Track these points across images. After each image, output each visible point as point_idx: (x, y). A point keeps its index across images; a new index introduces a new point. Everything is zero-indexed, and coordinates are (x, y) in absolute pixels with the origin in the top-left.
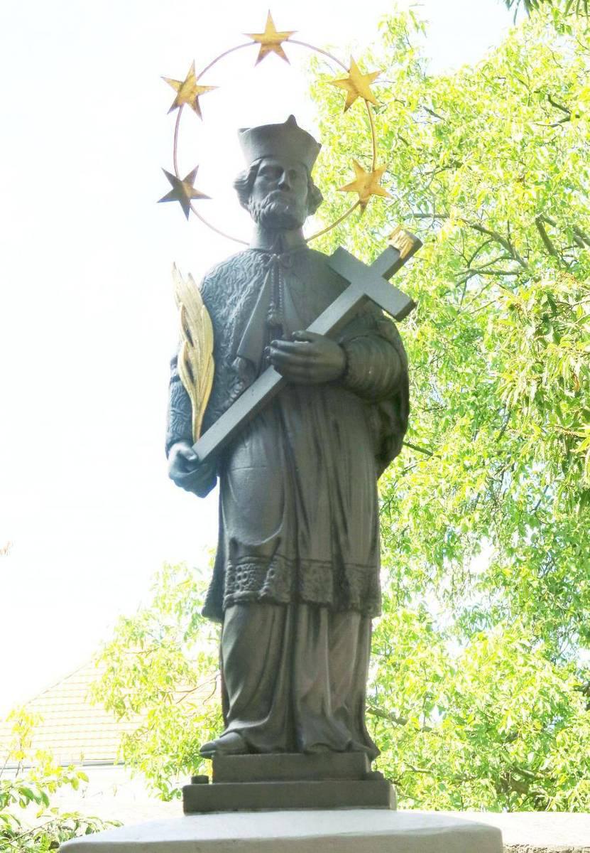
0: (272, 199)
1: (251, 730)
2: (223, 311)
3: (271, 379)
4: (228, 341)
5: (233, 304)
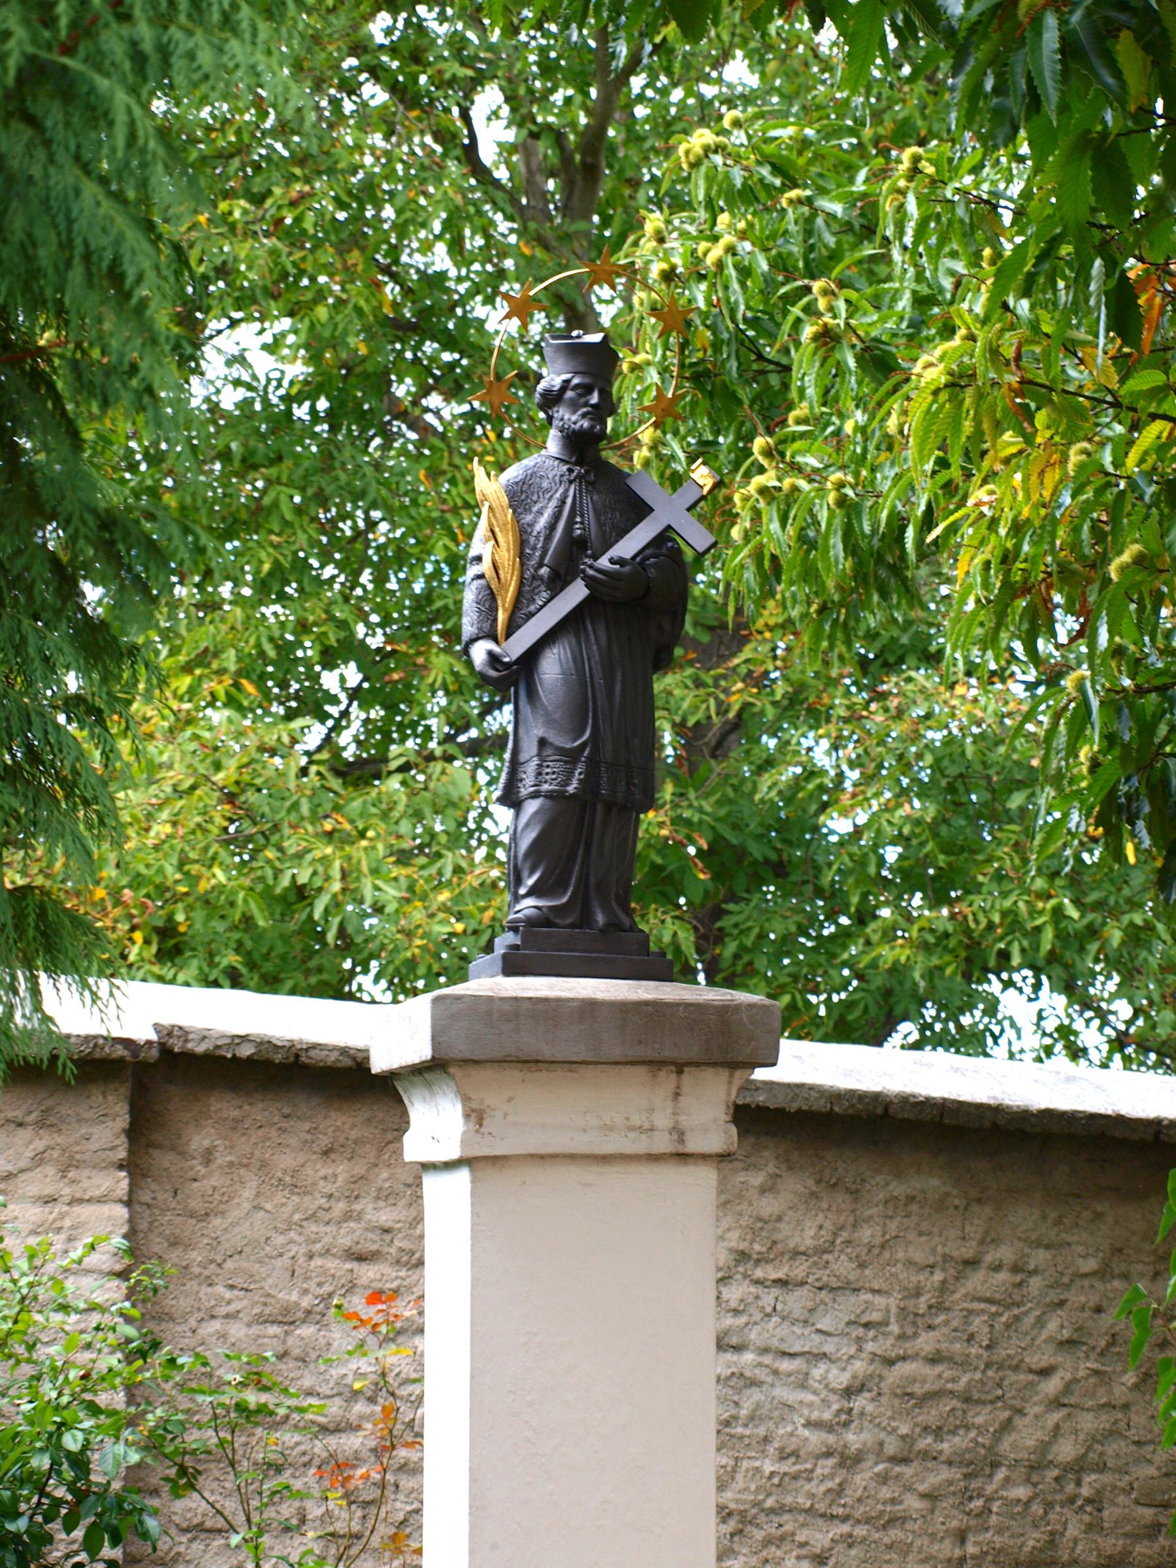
0: (584, 416)
1: (551, 908)
2: (529, 518)
3: (577, 592)
4: (534, 548)
5: (540, 513)
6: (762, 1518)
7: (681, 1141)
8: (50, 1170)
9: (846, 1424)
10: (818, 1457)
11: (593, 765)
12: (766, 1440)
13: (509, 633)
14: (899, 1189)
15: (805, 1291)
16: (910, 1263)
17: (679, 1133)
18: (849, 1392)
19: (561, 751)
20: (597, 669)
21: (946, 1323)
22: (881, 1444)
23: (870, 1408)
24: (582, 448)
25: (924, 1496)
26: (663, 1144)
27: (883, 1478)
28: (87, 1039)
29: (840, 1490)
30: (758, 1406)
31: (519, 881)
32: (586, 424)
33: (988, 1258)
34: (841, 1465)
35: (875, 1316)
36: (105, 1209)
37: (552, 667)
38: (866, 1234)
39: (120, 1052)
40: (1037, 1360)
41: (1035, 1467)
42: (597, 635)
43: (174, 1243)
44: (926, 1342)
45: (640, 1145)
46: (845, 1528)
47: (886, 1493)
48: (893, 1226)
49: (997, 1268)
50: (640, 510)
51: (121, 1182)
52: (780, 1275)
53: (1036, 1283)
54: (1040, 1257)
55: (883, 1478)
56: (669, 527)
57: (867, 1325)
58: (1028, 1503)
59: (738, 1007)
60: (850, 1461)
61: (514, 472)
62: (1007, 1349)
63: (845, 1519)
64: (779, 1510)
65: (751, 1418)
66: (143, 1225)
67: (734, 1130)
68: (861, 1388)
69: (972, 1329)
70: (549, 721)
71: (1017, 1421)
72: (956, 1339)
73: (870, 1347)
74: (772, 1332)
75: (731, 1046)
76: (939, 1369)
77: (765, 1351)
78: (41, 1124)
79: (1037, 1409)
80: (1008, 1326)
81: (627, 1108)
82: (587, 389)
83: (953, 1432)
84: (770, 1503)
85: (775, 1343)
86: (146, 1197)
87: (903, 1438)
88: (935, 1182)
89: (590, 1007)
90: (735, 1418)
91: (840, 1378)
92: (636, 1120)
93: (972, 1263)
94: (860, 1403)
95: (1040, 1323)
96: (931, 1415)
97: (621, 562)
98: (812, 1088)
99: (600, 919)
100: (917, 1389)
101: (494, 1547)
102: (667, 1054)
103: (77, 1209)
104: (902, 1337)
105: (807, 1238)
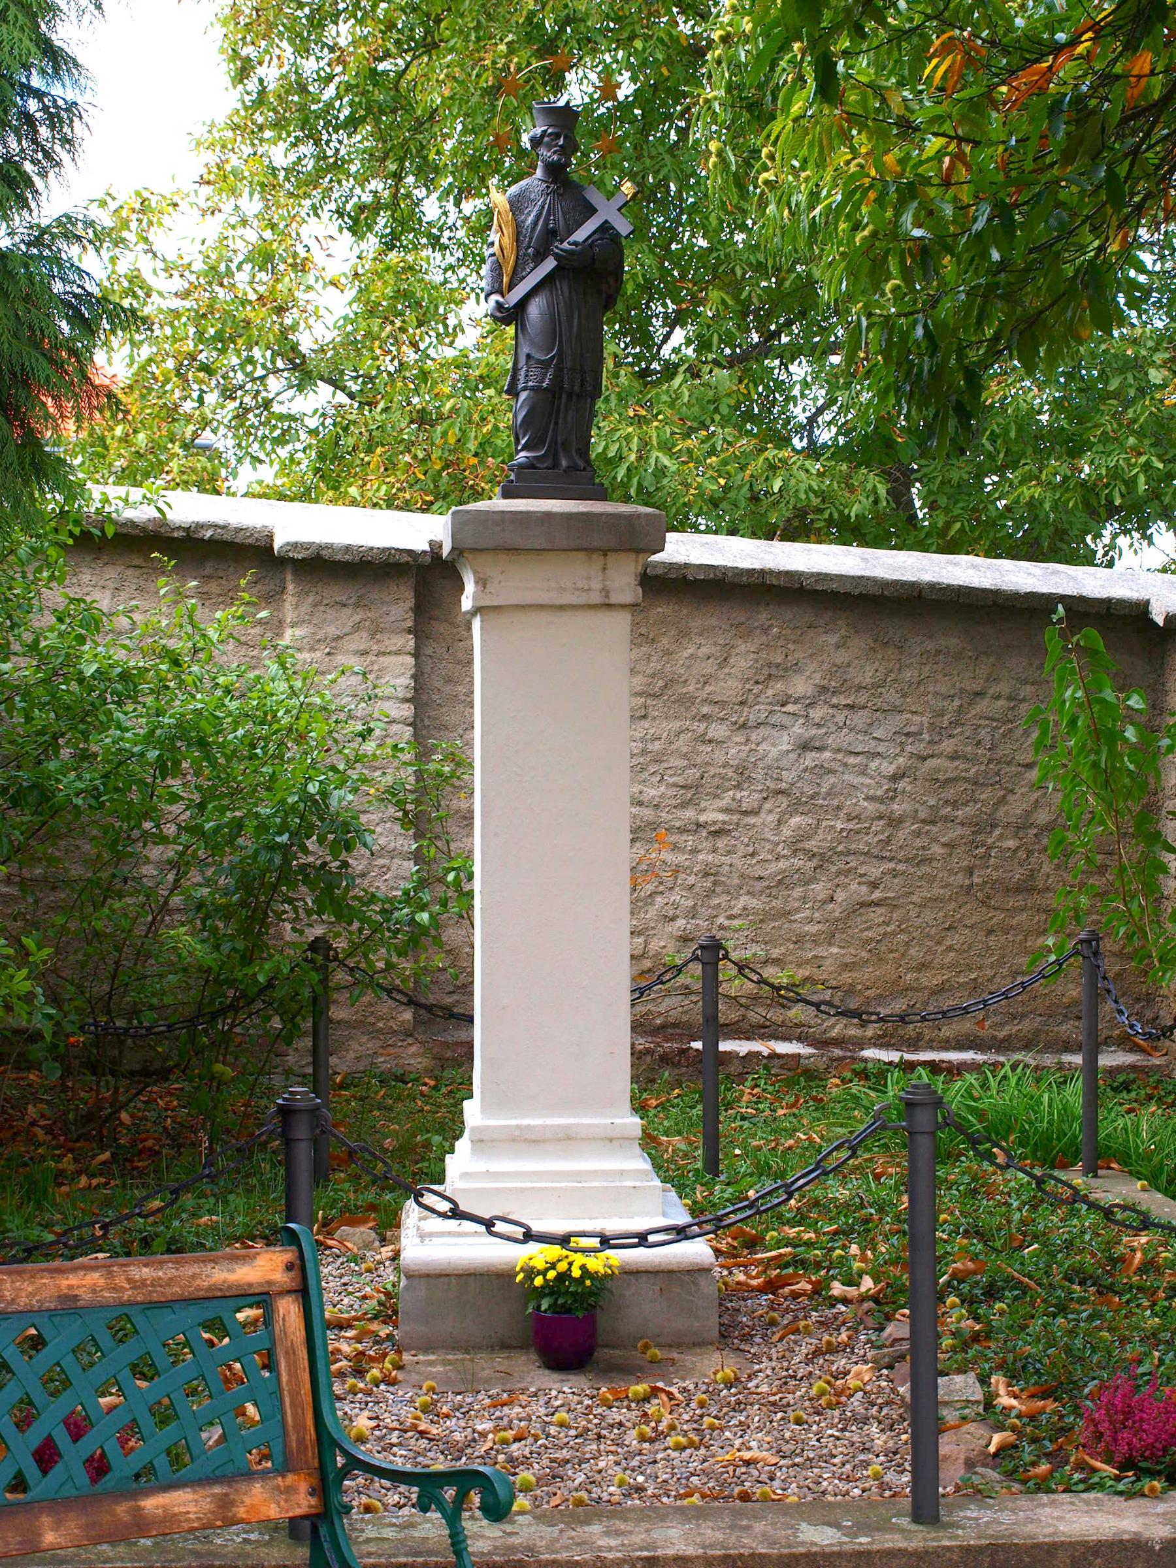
3: (550, 264)
5: (529, 214)
6: (835, 858)
7: (607, 596)
8: (364, 634)
9: (893, 799)
10: (873, 819)
11: (559, 370)
12: (838, 808)
13: (511, 287)
14: (930, 646)
15: (865, 712)
16: (937, 694)
17: (606, 592)
18: (894, 778)
19: (539, 362)
20: (562, 310)
21: (962, 733)
22: (916, 811)
23: (909, 788)
24: (556, 172)
25: (944, 845)
26: (595, 598)
27: (917, 834)
28: (384, 550)
29: (888, 841)
30: (833, 786)
31: (517, 441)
32: (555, 157)
33: (991, 691)
34: (889, 825)
35: (913, 729)
36: (400, 658)
37: (534, 310)
38: (907, 675)
39: (405, 558)
40: (1022, 758)
41: (1021, 826)
42: (563, 287)
43: (448, 681)
44: (947, 746)
45: (582, 599)
46: (891, 865)
47: (919, 843)
48: (926, 671)
49: (998, 697)
50: (591, 211)
51: (410, 642)
52: (849, 702)
53: (1024, 707)
54: (1027, 690)
55: (917, 834)
56: (606, 222)
57: (907, 735)
58: (1016, 851)
59: (639, 516)
60: (895, 822)
61: (514, 189)
62: (1003, 751)
63: (891, 859)
64: (848, 853)
65: (828, 794)
66: (427, 669)
67: (640, 590)
68: (903, 776)
69: (980, 737)
70: (532, 344)
71: (1010, 798)
72: (967, 744)
73: (909, 748)
74: (844, 739)
75: (639, 539)
76: (956, 763)
77: (839, 750)
78: (357, 605)
79: (1023, 790)
80: (1004, 735)
81: (574, 577)
82: (557, 136)
83: (965, 804)
84: (840, 848)
85: (845, 745)
86: (429, 651)
87: (931, 807)
88: (955, 641)
89: (548, 516)
90: (818, 794)
91: (889, 769)
92: (579, 585)
93: (980, 694)
94: (902, 785)
95: (1027, 733)
96: (950, 793)
97: (575, 243)
98: (869, 579)
99: (564, 463)
100: (941, 777)
101: (496, 834)
102: (596, 544)
103: (382, 659)
104: (930, 742)
105: (868, 677)
